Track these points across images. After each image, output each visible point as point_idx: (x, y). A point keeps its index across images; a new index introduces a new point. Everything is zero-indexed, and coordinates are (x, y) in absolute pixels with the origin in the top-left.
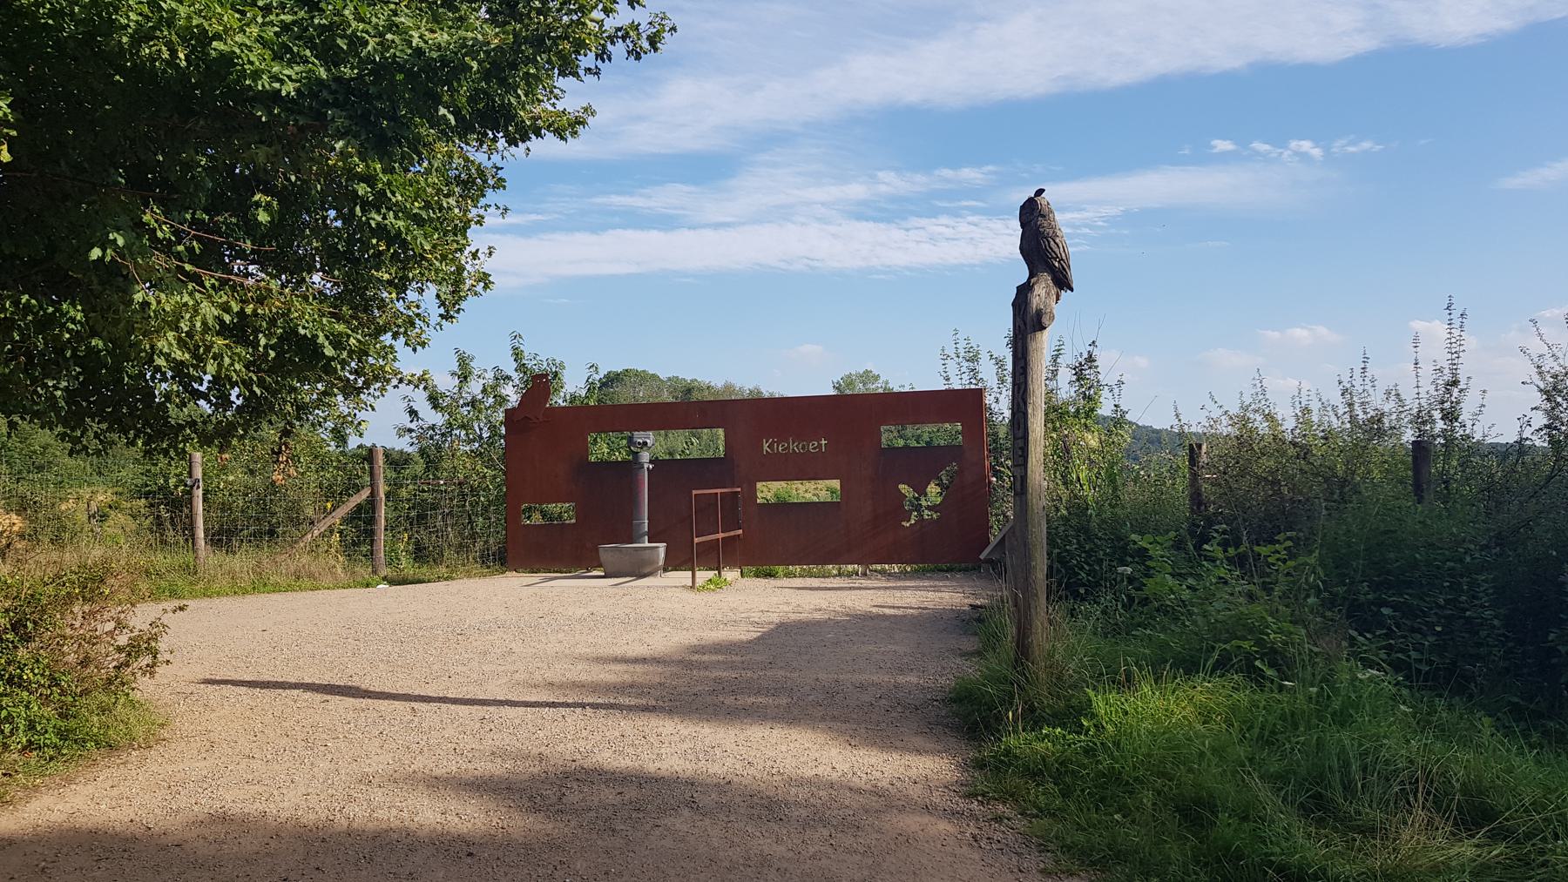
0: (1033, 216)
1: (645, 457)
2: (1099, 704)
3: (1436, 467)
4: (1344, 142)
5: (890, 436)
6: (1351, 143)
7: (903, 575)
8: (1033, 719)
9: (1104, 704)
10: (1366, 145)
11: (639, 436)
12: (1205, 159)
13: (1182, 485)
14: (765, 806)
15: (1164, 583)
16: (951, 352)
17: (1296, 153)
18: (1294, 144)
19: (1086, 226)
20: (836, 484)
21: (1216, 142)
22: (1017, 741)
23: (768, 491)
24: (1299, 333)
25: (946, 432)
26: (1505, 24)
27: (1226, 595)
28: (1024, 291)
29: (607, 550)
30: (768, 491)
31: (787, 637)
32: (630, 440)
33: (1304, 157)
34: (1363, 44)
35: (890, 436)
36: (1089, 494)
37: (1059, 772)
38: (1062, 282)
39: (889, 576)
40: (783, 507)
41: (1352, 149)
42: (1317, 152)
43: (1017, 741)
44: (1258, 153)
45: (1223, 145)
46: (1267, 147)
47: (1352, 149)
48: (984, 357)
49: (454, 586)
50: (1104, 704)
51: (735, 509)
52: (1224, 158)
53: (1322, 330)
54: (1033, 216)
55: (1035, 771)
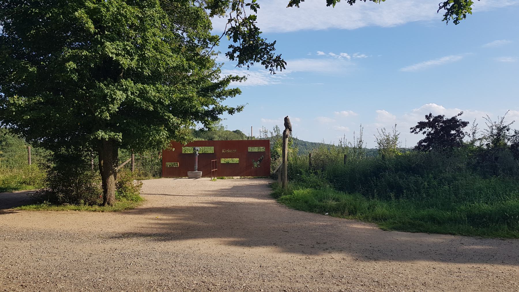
0: (286, 119)
1: (197, 152)
2: (295, 192)
3: (347, 159)
4: (356, 54)
5: (251, 149)
6: (359, 55)
7: (252, 179)
8: (285, 194)
9: (295, 192)
10: (363, 56)
11: (197, 148)
12: (315, 57)
13: (308, 160)
14: (252, 204)
15: (304, 176)
16: (262, 131)
17: (343, 57)
18: (342, 54)
19: (280, 76)
20: (238, 159)
21: (318, 52)
22: (284, 197)
23: (223, 161)
24: (345, 112)
25: (262, 149)
26: (401, 22)
27: (313, 178)
28: (285, 131)
29: (189, 173)
30: (223, 161)
31: (235, 187)
32: (194, 149)
33: (345, 58)
34: (361, 24)
35: (251, 149)
36: (292, 163)
37: (290, 200)
38: (290, 130)
39: (249, 178)
40: (228, 164)
41: (359, 57)
42: (348, 57)
43: (284, 197)
44: (331, 56)
45: (321, 53)
46: (334, 54)
47: (359, 57)
48: (269, 132)
49: (160, 179)
50: (295, 192)
51: (217, 164)
52: (321, 57)
53: (351, 112)
54: (286, 119)
55: (287, 200)
